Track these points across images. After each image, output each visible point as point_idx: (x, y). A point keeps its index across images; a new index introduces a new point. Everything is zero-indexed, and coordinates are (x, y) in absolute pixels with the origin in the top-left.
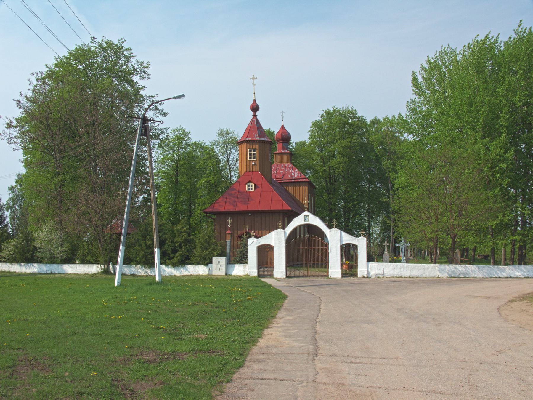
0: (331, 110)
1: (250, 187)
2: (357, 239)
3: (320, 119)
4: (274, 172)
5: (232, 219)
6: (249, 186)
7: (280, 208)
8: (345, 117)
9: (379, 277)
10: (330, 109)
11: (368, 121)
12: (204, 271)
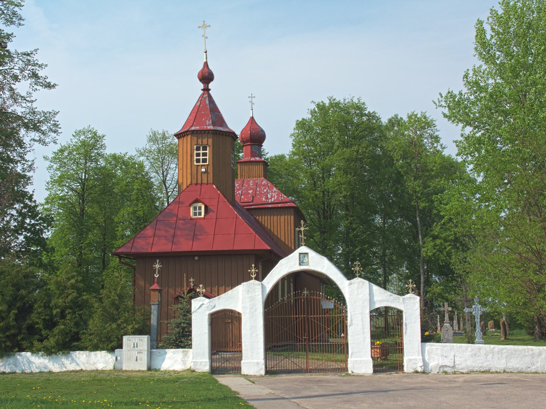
0: (327, 103)
1: (198, 211)
2: (401, 298)
3: (310, 116)
4: (238, 192)
5: (161, 263)
6: (195, 208)
7: (248, 246)
8: (348, 113)
9: (446, 373)
10: (325, 102)
11: (384, 120)
12: (106, 362)
